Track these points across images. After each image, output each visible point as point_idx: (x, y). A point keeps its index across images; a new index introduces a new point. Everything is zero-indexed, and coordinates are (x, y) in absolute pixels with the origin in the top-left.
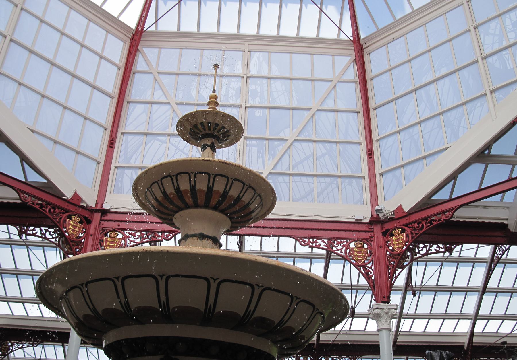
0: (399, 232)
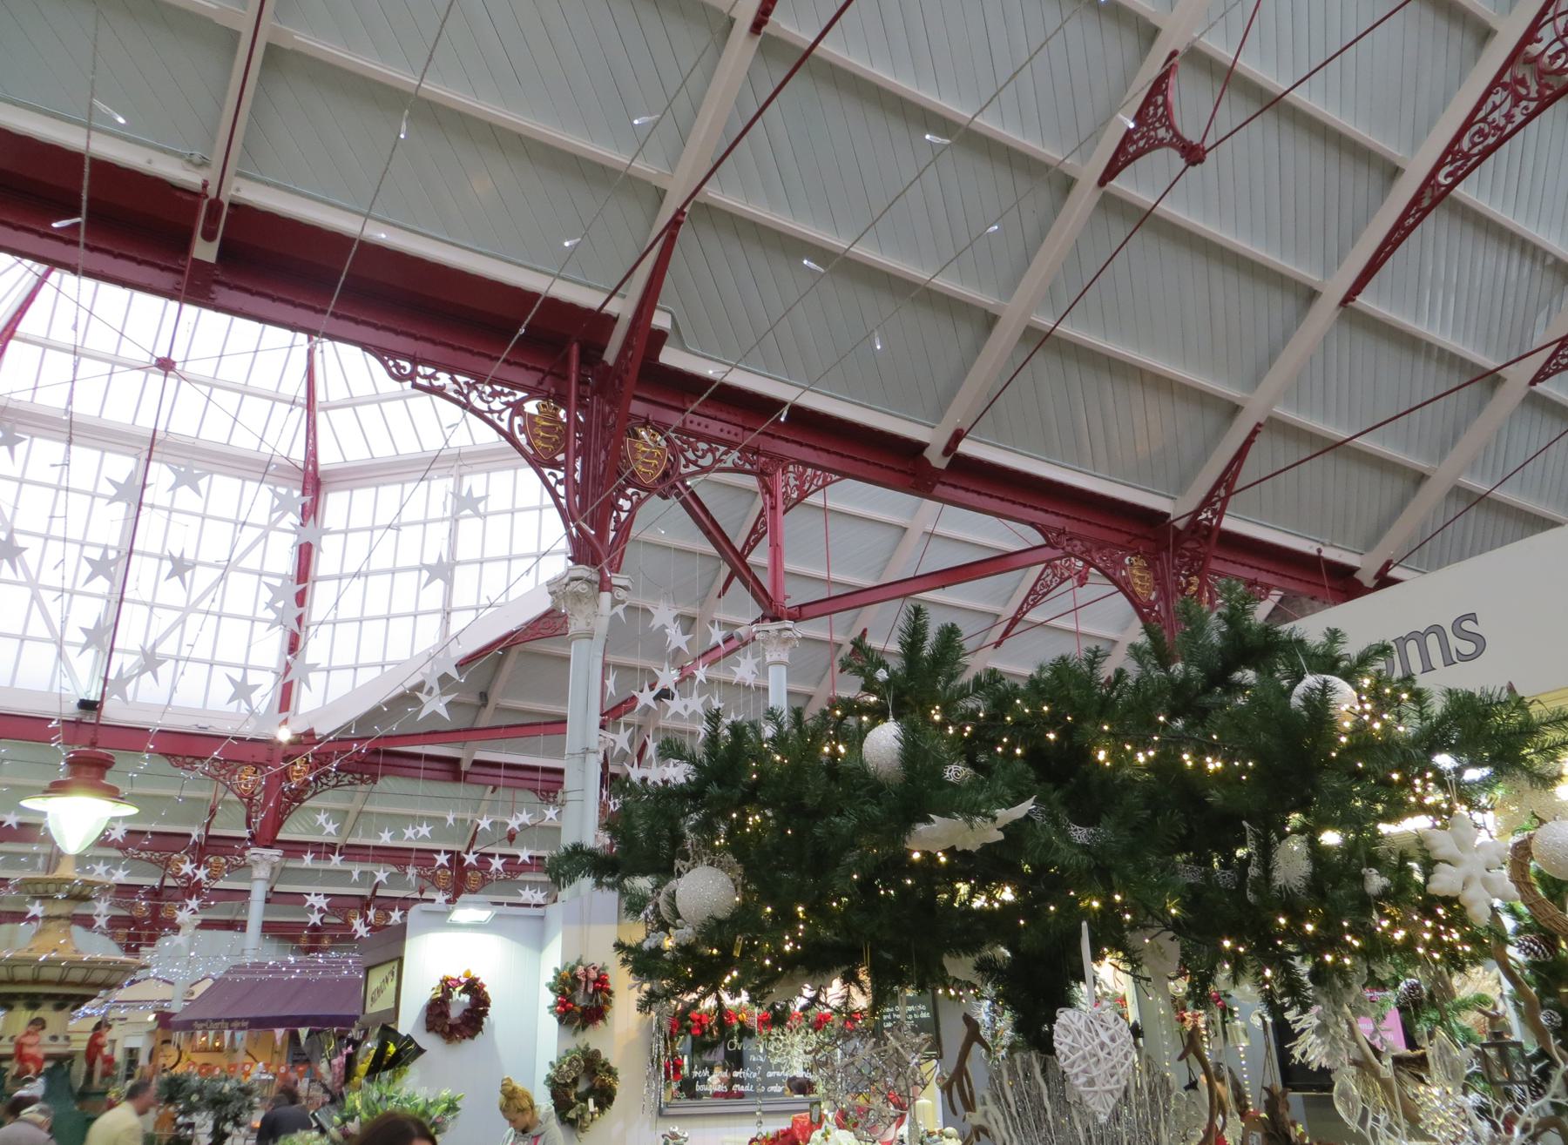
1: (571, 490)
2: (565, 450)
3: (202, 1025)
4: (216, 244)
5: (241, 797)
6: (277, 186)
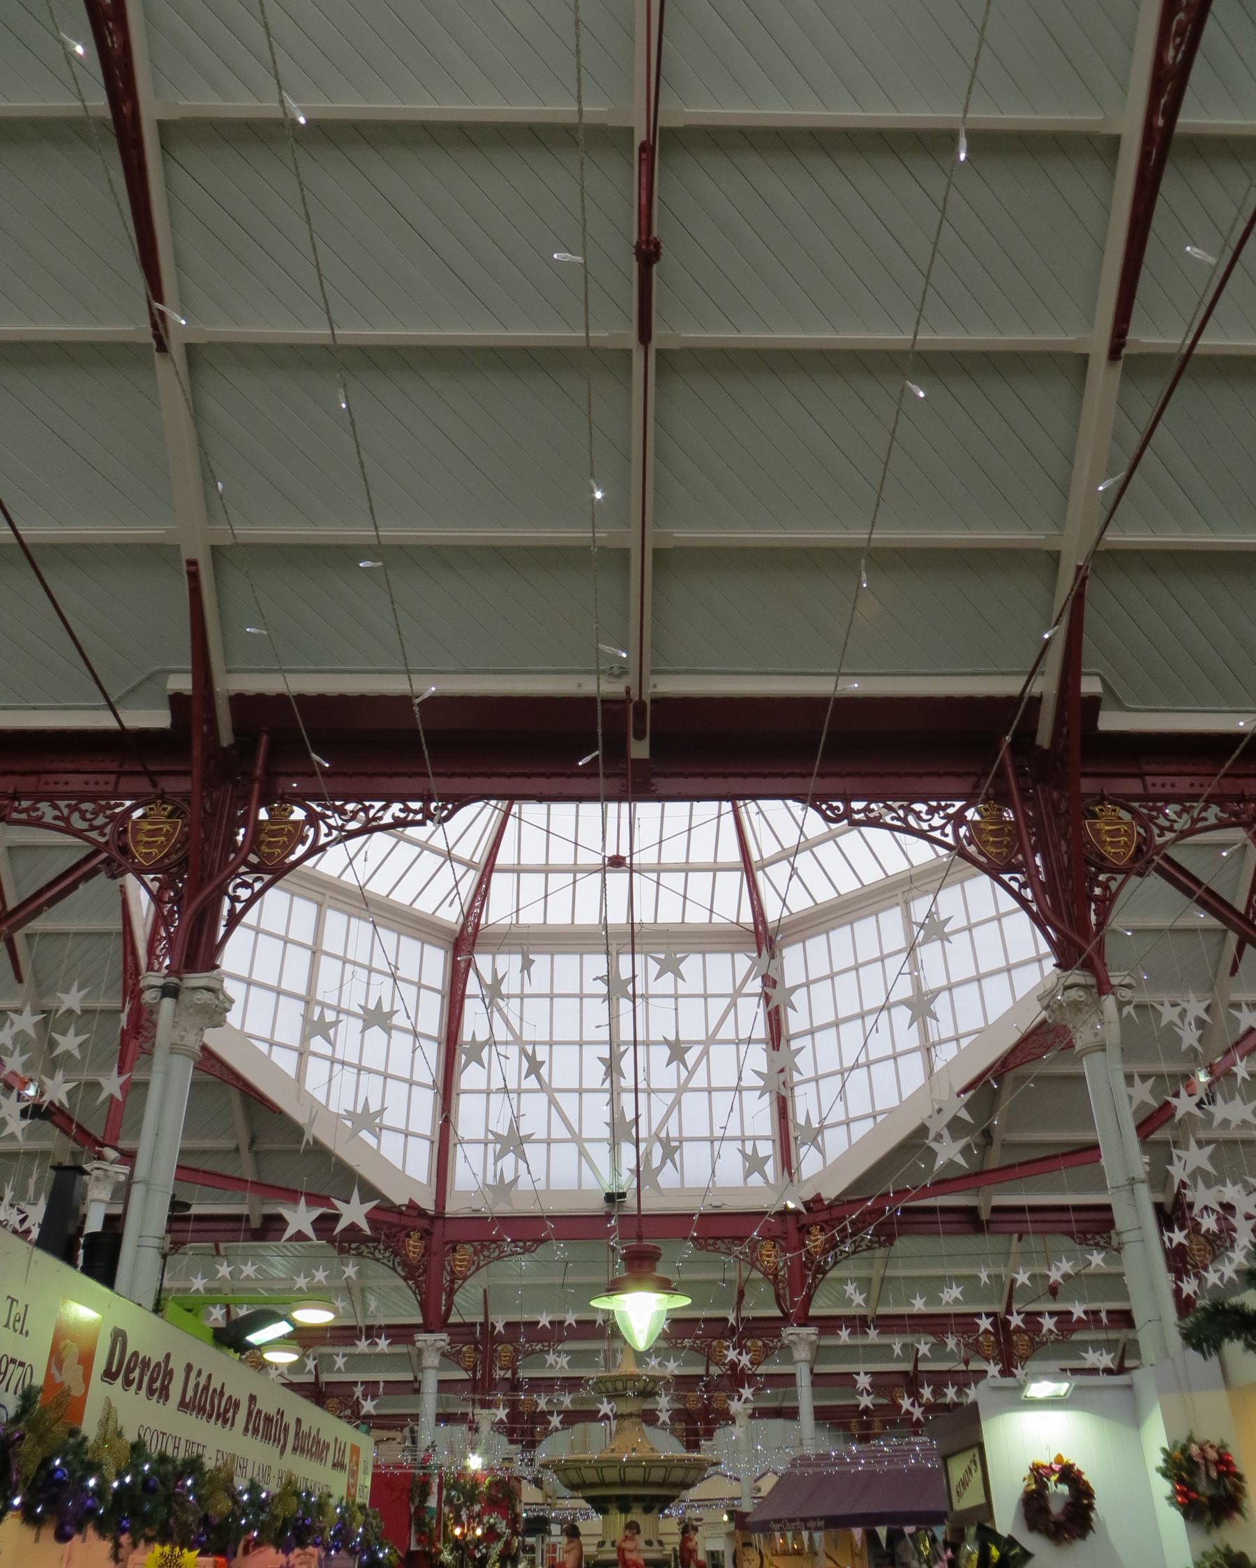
1: (1039, 893)
2: (1021, 850)
3: (777, 1526)
4: (647, 740)
5: (765, 1274)
6: (687, 672)
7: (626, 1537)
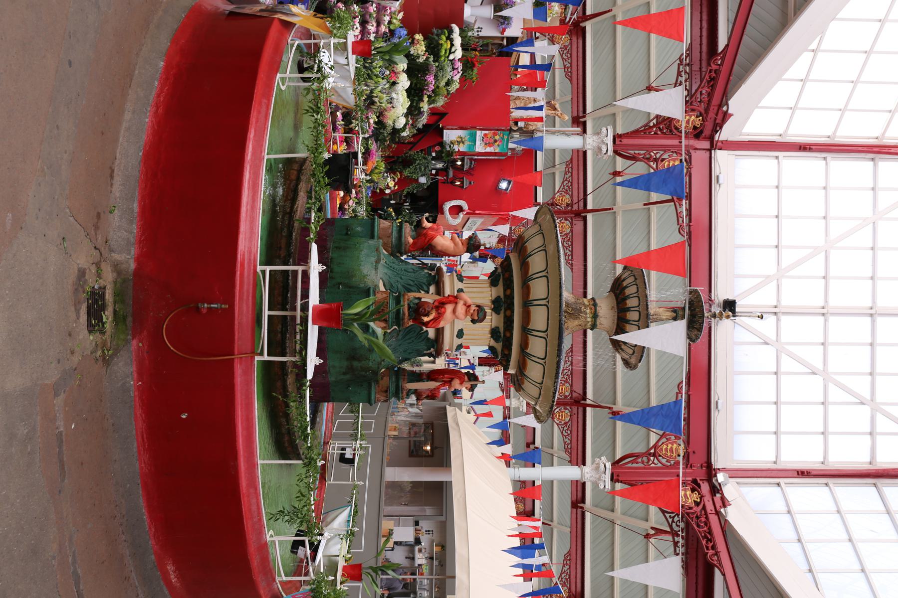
0: (696, 500)
5: (655, 446)
7: (469, 306)
